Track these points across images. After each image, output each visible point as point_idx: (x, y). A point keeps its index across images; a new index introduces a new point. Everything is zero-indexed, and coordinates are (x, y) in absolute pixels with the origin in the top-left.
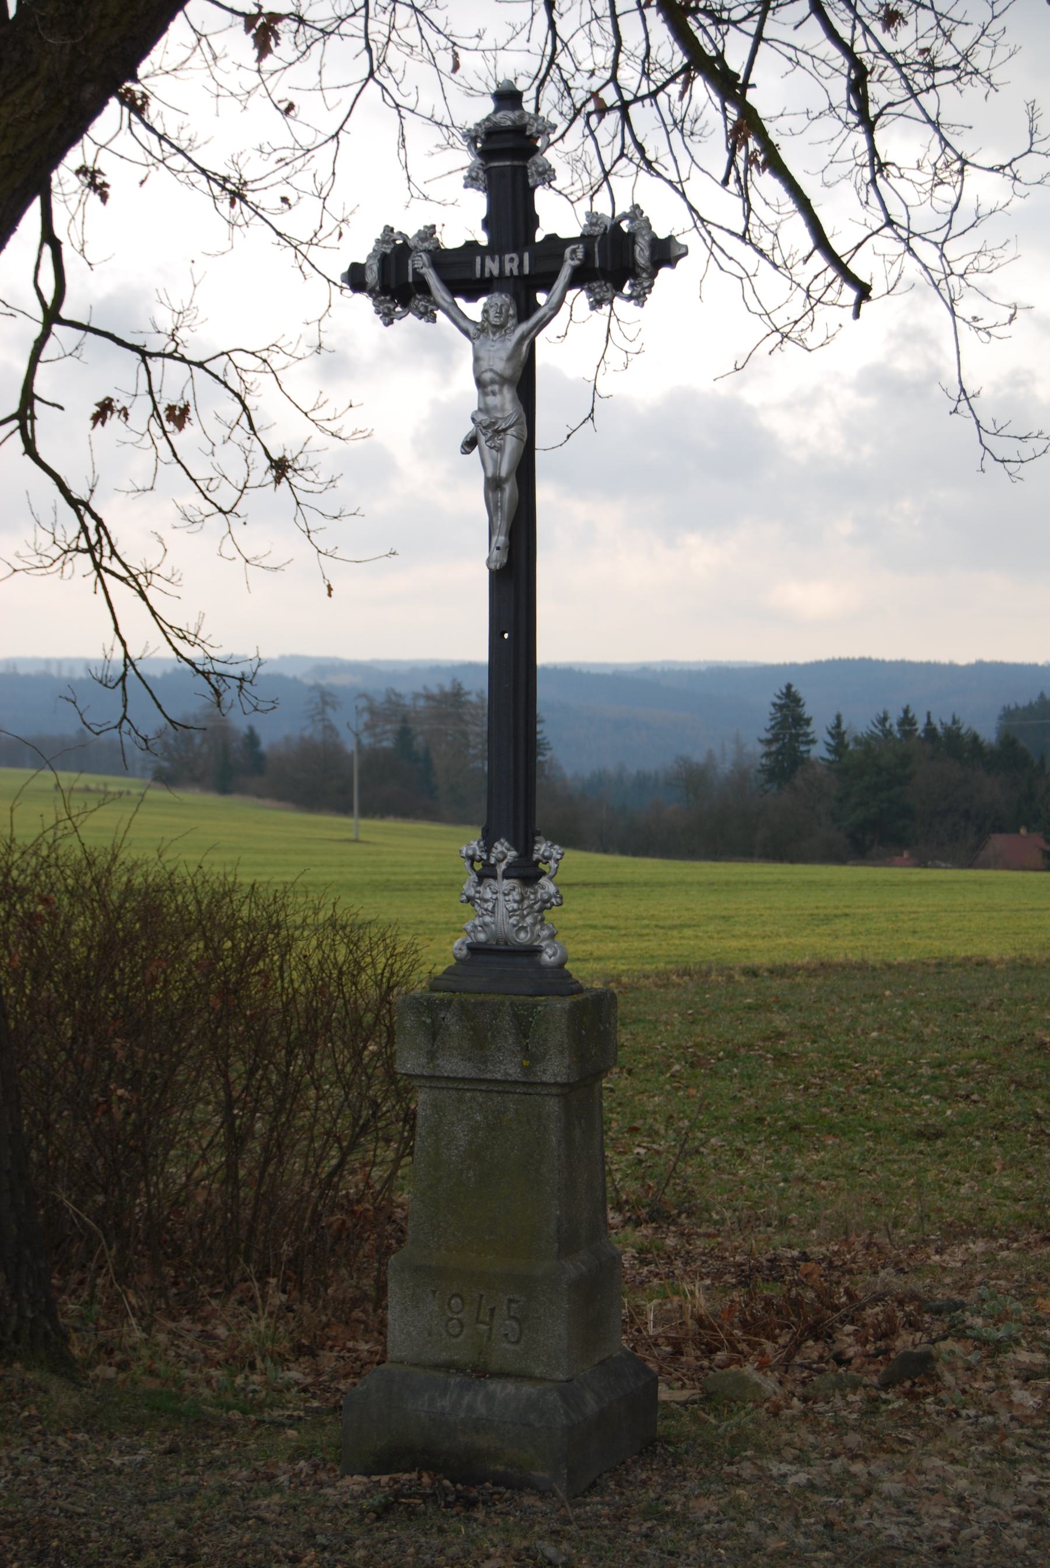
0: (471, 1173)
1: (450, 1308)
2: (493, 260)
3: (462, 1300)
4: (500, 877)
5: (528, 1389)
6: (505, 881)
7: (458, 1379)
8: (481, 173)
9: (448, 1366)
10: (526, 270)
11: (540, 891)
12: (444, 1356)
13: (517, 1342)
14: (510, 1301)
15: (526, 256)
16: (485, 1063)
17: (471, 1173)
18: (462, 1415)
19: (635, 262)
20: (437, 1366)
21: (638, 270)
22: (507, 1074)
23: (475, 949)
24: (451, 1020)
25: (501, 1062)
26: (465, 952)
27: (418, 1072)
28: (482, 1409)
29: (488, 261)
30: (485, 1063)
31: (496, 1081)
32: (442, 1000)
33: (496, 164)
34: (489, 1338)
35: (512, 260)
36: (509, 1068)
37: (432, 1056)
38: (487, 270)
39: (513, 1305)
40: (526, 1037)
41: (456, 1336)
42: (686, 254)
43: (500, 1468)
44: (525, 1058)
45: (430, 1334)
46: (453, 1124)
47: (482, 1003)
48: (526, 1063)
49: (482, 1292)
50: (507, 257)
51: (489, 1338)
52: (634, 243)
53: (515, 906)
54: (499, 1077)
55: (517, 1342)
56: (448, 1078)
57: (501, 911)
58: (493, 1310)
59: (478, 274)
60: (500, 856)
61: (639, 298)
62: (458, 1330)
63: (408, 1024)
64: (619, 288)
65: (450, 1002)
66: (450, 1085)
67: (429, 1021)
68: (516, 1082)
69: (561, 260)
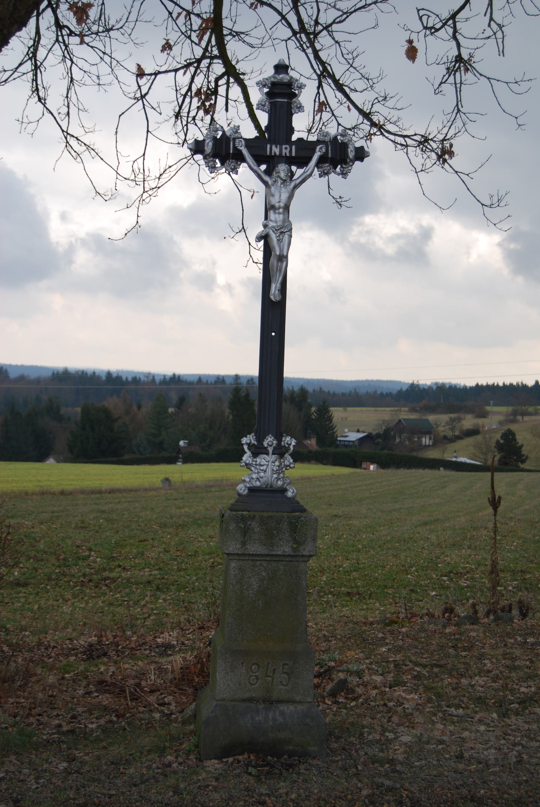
2: (276, 147)
3: (258, 666)
4: (270, 454)
5: (300, 707)
8: (267, 103)
9: (250, 700)
10: (294, 154)
11: (286, 461)
12: (247, 695)
13: (287, 685)
14: (284, 664)
15: (294, 147)
18: (271, 723)
19: (348, 156)
20: (244, 700)
21: (348, 160)
22: (284, 551)
23: (252, 490)
24: (254, 525)
25: (281, 546)
26: (246, 492)
27: (236, 552)
28: (280, 719)
29: (274, 147)
31: (278, 555)
32: (249, 515)
33: (280, 100)
34: (272, 684)
35: (286, 148)
36: (286, 549)
37: (244, 544)
38: (273, 152)
39: (286, 667)
41: (253, 685)
42: (369, 156)
43: (291, 748)
44: (294, 543)
45: (240, 685)
46: (250, 578)
47: (271, 517)
48: (294, 546)
49: (269, 661)
50: (284, 147)
51: (272, 684)
52: (348, 147)
54: (280, 553)
55: (287, 685)
56: (253, 555)
58: (274, 670)
59: (268, 153)
60: (270, 443)
61: (344, 174)
62: (255, 681)
63: (231, 528)
64: (335, 168)
65: (254, 517)
66: (250, 558)
67: (243, 526)
68: (289, 555)
69: (314, 152)
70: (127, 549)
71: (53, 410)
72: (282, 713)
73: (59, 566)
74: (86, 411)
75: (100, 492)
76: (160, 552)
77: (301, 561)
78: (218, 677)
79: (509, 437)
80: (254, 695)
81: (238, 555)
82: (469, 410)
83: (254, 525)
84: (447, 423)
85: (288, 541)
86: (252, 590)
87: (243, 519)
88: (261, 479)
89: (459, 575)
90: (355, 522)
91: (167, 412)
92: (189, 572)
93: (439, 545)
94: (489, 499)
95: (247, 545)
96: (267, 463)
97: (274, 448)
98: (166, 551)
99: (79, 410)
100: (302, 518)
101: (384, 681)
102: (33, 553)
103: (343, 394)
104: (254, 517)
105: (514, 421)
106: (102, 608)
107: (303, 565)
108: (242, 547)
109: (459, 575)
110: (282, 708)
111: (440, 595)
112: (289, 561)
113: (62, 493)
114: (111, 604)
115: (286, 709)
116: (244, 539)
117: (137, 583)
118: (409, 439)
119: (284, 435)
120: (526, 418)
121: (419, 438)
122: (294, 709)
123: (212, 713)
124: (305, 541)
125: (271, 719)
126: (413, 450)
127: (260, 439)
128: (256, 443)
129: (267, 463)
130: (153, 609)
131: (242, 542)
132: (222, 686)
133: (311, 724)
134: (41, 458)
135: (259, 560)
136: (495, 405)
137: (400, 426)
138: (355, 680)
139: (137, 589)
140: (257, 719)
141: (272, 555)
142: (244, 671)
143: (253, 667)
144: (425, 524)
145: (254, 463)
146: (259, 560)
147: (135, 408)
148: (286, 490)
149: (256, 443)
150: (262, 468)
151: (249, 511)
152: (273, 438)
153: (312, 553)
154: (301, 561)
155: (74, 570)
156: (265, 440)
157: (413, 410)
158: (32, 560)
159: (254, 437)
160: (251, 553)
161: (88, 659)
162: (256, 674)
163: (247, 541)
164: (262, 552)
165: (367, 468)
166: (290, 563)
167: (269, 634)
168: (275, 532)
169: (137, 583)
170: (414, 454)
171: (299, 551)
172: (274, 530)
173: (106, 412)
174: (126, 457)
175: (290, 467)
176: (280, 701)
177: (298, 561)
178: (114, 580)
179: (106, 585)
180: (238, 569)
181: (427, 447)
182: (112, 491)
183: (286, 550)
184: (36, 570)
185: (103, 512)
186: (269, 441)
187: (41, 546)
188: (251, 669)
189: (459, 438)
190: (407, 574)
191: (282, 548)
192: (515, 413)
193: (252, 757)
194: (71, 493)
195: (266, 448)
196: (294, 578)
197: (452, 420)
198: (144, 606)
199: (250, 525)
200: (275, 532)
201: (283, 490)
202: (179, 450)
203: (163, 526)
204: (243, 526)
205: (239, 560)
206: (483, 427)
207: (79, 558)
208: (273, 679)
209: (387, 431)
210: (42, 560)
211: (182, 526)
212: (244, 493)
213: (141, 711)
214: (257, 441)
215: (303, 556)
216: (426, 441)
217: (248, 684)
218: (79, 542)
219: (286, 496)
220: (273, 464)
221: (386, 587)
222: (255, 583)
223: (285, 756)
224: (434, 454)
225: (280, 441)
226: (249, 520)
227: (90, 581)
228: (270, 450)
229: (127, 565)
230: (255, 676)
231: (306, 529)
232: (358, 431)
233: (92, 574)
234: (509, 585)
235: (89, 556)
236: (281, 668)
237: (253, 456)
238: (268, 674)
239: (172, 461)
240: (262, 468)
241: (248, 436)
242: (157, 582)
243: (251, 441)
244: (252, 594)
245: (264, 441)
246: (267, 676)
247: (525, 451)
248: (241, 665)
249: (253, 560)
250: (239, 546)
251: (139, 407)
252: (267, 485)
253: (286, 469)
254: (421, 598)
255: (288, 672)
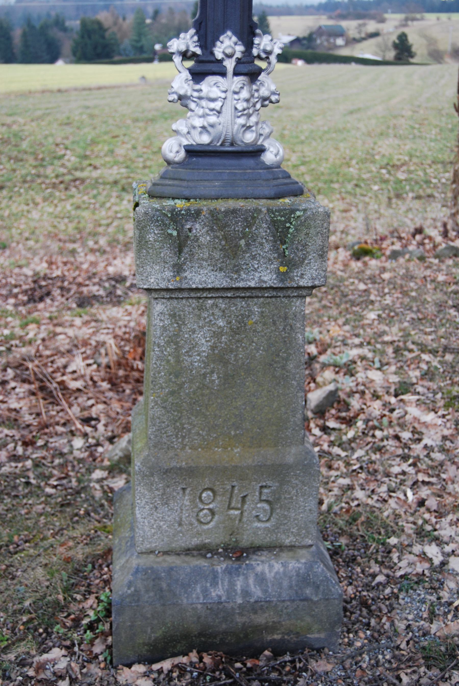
0: (215, 376)
1: (201, 500)
6: (235, 78)
7: (224, 566)
9: (202, 550)
12: (195, 541)
13: (268, 520)
14: (262, 487)
16: (237, 272)
17: (215, 376)
20: (188, 551)
23: (192, 152)
25: (255, 270)
26: (182, 154)
28: (257, 592)
30: (237, 272)
31: (250, 288)
32: (188, 210)
34: (240, 520)
36: (264, 274)
37: (178, 269)
39: (265, 491)
40: (283, 243)
43: (277, 637)
44: (282, 264)
46: (194, 331)
47: (234, 211)
48: (282, 269)
49: (235, 483)
53: (245, 105)
55: (268, 520)
56: (197, 289)
57: (228, 112)
58: (244, 498)
60: (229, 51)
62: (209, 518)
63: (151, 237)
66: (193, 295)
67: (175, 233)
68: (272, 288)
70: (100, 147)
71: (59, 23)
72: (261, 579)
73: (35, 167)
74: (84, 24)
75: (90, 89)
76: (128, 149)
77: (294, 297)
78: (138, 516)
79: (403, 38)
80: (207, 541)
81: (167, 290)
82: (372, 17)
83: (198, 229)
84: (356, 28)
85: (270, 260)
86: (199, 355)
87: (176, 217)
88: (209, 129)
89: (396, 167)
90: (294, 113)
91: (144, 22)
92: (153, 169)
93: (369, 134)
94: (455, 105)
95: (185, 271)
96: (223, 95)
97: (239, 61)
98: (134, 148)
99: (78, 22)
100: (298, 213)
101: (386, 385)
102: (14, 154)
103: (278, 7)
104: (198, 213)
105: (405, 25)
106: (69, 212)
107: (298, 303)
108: (175, 276)
109: (396, 167)
110: (259, 569)
111: (382, 189)
112: (271, 297)
113: (59, 91)
114: (78, 207)
115: (267, 571)
116: (179, 258)
117: (104, 184)
118: (328, 41)
119: (258, 31)
120: (415, 23)
121: (335, 40)
122: (282, 570)
123: (129, 588)
124: (304, 259)
125: (239, 591)
126: (330, 49)
127: (207, 40)
128: (198, 51)
129: (223, 95)
130: (116, 212)
131: (174, 266)
132: (147, 529)
133: (315, 599)
134: (52, 60)
135: (212, 298)
136: (393, 12)
137: (320, 31)
138: (347, 383)
139: (104, 190)
140: (213, 594)
141: (238, 289)
142: (188, 503)
143: (204, 495)
144: (351, 113)
145: (196, 94)
146: (212, 298)
147: (121, 20)
148: (261, 150)
149: (198, 51)
150: (212, 105)
151: (188, 199)
152: (234, 39)
153: (317, 283)
154: (294, 297)
155: (49, 171)
156: (218, 43)
157: (330, 18)
158: (12, 161)
159: (196, 38)
160: (194, 286)
161: (29, 301)
162: (211, 506)
163: (185, 264)
164: (217, 285)
165: (296, 64)
166: (274, 300)
167: (233, 433)
168: (242, 242)
169: (104, 184)
170: (331, 52)
171: (292, 279)
172: (241, 239)
173: (99, 23)
174: (116, 58)
175: (271, 102)
176: (256, 549)
177: (289, 297)
178: (83, 181)
179: (75, 187)
180: (170, 315)
181: (340, 47)
182: (99, 88)
183: (266, 279)
184: (14, 170)
185: (88, 108)
186: (227, 45)
187: (24, 145)
188: (200, 497)
189: (363, 39)
190: (349, 167)
191: (257, 275)
192: (407, 19)
193: (207, 659)
194: (66, 91)
195: (220, 62)
196: (281, 328)
197: (360, 25)
198: (110, 208)
199: (190, 230)
200: (242, 242)
201: (258, 151)
202: (155, 53)
203: (136, 120)
204: (175, 233)
205: (172, 298)
206: (383, 30)
207: (55, 158)
208: (242, 513)
209: (311, 35)
210: (22, 160)
211: (152, 120)
212: (177, 159)
213: (59, 432)
214: (201, 47)
215: (299, 288)
216: (340, 41)
217: (196, 523)
218: (59, 140)
219: (263, 163)
220: (236, 97)
221: (332, 182)
222: (203, 341)
223: (267, 653)
224: (345, 52)
225: (249, 45)
226: (187, 221)
227: (62, 182)
228: (230, 65)
229: (97, 162)
230: (209, 509)
231: (307, 234)
232: (289, 35)
233: (64, 175)
234: (441, 178)
235: (64, 155)
236: (257, 494)
237: (193, 79)
238: (233, 505)
239: (150, 60)
240: (212, 105)
241: (182, 35)
242: (124, 181)
243: (188, 47)
244: (199, 361)
245: (214, 46)
246: (229, 508)
247: (414, 49)
248: (181, 492)
249: (200, 298)
250: (168, 274)
251: (124, 19)
252: (223, 142)
253: (263, 106)
254: (365, 193)
255: (270, 499)
